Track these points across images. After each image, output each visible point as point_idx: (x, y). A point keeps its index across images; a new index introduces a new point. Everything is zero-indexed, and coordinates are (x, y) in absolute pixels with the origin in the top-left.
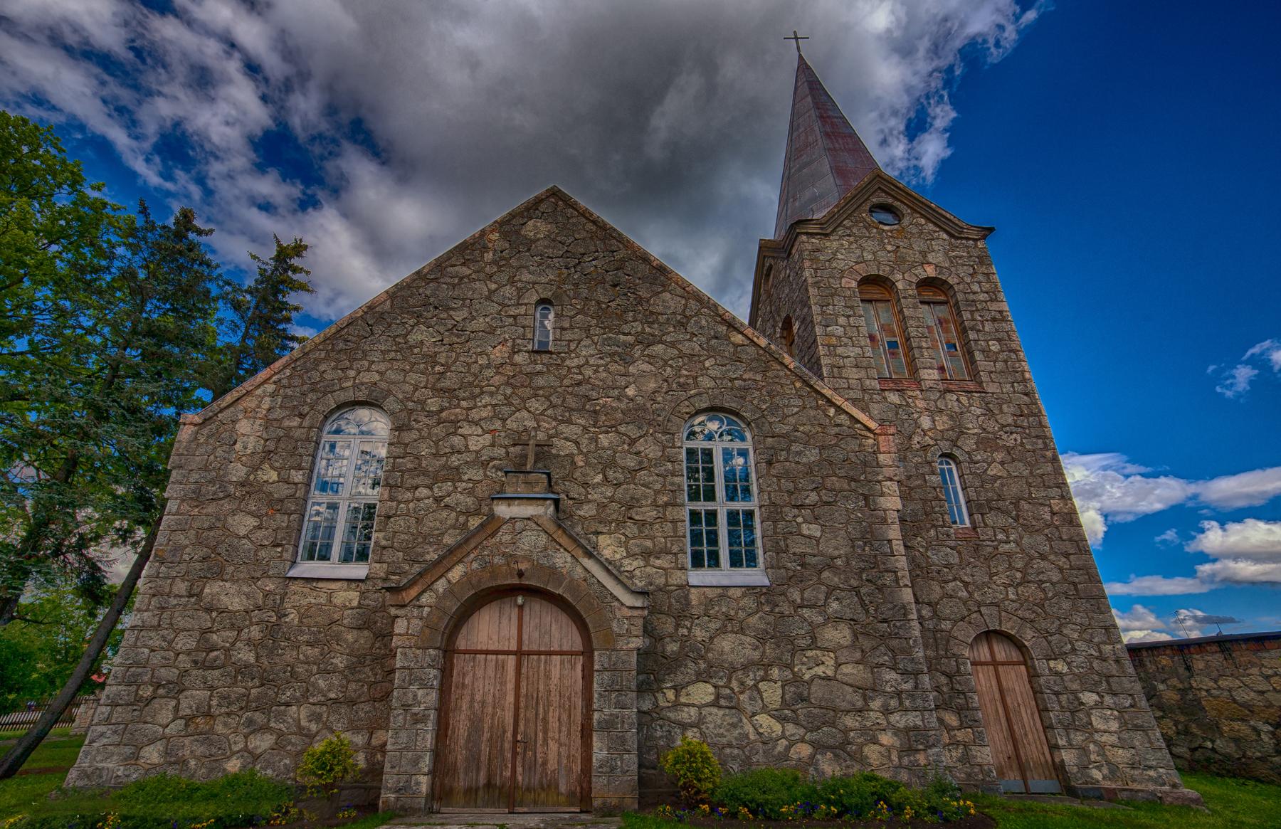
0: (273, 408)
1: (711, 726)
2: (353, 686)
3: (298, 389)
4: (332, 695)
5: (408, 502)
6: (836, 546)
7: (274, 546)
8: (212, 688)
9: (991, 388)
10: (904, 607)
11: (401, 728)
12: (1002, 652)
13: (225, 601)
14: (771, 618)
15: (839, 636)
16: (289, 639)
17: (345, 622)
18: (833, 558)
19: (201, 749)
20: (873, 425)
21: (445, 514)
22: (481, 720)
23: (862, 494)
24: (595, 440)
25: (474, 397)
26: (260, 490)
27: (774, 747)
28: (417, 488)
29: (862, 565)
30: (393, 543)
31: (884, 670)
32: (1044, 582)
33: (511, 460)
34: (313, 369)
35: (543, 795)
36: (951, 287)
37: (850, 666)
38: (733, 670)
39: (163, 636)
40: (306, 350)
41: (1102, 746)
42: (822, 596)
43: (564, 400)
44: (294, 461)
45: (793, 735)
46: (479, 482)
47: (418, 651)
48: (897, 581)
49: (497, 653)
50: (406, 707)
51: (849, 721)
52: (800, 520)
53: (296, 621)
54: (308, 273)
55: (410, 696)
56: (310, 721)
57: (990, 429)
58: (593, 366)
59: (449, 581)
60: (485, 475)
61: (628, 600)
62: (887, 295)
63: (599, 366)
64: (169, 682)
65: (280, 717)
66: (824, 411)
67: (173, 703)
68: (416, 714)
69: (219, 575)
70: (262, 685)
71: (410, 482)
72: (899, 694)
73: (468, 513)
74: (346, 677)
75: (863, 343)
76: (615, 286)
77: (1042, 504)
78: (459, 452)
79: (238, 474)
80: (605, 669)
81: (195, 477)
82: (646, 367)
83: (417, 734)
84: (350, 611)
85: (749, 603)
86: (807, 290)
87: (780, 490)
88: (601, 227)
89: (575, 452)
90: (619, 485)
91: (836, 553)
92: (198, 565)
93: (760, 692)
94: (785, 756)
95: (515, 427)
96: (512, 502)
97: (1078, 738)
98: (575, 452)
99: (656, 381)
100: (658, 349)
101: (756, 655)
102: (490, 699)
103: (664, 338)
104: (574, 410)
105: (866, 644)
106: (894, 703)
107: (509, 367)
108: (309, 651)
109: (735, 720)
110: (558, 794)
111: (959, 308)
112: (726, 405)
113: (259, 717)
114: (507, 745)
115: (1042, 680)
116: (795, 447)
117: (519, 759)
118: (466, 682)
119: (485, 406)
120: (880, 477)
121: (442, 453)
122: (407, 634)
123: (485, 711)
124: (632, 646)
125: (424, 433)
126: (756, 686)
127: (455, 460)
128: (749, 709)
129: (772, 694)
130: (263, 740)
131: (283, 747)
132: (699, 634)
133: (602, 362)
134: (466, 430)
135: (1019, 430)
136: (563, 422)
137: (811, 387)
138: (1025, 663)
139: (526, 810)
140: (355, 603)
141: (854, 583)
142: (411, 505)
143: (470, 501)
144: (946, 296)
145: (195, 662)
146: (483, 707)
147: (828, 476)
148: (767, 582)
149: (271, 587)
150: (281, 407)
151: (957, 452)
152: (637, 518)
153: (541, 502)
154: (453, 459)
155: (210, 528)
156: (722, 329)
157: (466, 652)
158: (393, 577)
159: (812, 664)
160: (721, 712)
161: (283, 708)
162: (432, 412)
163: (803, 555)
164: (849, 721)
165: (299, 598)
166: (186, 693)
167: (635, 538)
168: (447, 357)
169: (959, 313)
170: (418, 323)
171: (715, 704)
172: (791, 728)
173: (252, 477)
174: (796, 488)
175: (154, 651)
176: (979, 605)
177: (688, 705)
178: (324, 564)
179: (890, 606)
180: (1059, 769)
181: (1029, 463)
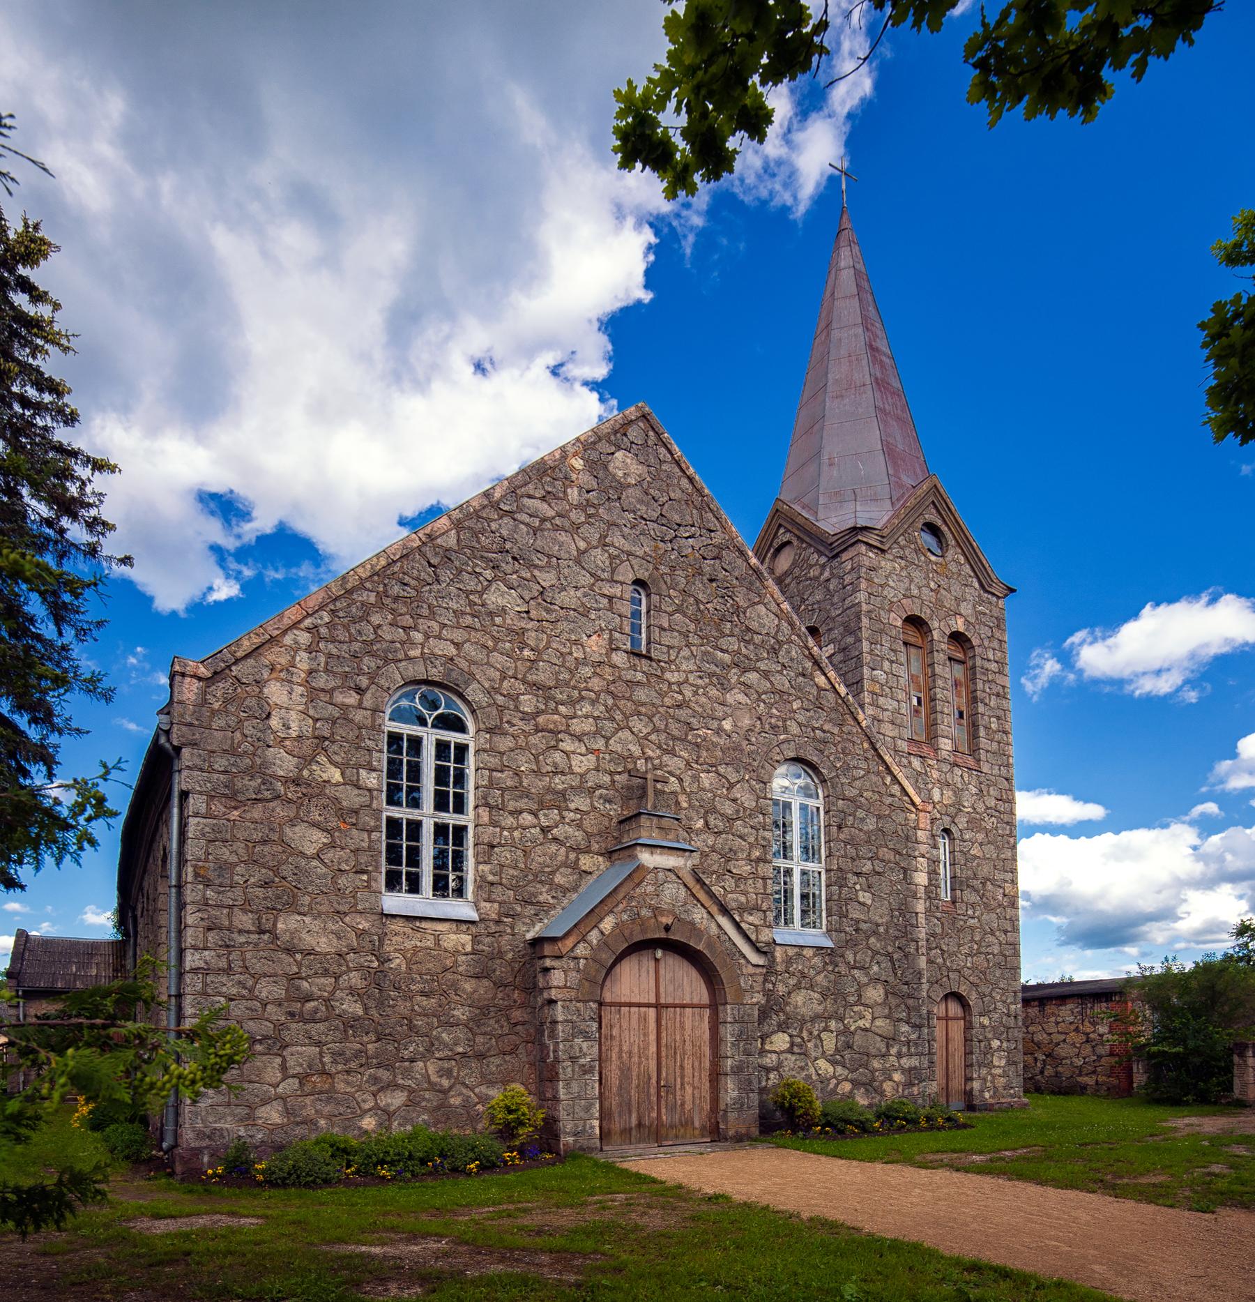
0: (316, 671)
1: (787, 1069)
2: (480, 1039)
3: (345, 647)
4: (460, 1050)
5: (511, 829)
6: (880, 915)
7: (356, 872)
8: (319, 1044)
9: (985, 768)
10: (920, 973)
11: (571, 1079)
12: (954, 1008)
13: (308, 940)
14: (832, 977)
15: (876, 995)
16: (400, 988)
17: (460, 969)
18: (878, 925)
19: (329, 1108)
20: (917, 800)
21: (553, 847)
22: (629, 1069)
23: (903, 868)
24: (696, 778)
25: (572, 703)
26: (321, 794)
27: (828, 1085)
28: (521, 812)
29: (897, 933)
30: (501, 878)
31: (902, 1024)
32: (989, 954)
33: (617, 790)
34: (361, 619)
35: (682, 1131)
36: (973, 647)
37: (880, 1020)
38: (803, 1022)
39: (240, 983)
40: (349, 586)
41: (993, 1076)
42: (868, 959)
43: (667, 725)
44: (362, 757)
45: (840, 1075)
46: (587, 813)
47: (578, 1004)
48: (917, 950)
49: (639, 1005)
50: (573, 1059)
51: (876, 1064)
52: (858, 887)
53: (404, 967)
54: (57, 307)
55: (577, 1048)
56: (441, 1076)
57: (978, 810)
58: (692, 685)
59: (602, 933)
60: (592, 805)
61: (755, 958)
62: (920, 641)
63: (698, 687)
64: (266, 1037)
65: (407, 1073)
66: (883, 779)
67: (278, 1060)
68: (583, 1066)
69: (292, 906)
70: (379, 1040)
71: (512, 805)
72: (908, 1042)
73: (578, 850)
74: (471, 1029)
75: (900, 697)
76: (711, 580)
77: (1000, 886)
78: (563, 773)
79: (285, 766)
80: (736, 1022)
81: (220, 763)
82: (741, 698)
83: (586, 1084)
84: (464, 957)
85: (817, 961)
86: (860, 619)
87: (845, 856)
88: (698, 490)
89: (679, 790)
90: (718, 833)
91: (880, 921)
92: (260, 892)
93: (822, 1041)
94: (834, 1091)
95: (619, 749)
96: (654, 850)
97: (984, 1071)
98: (679, 790)
99: (751, 718)
100: (752, 677)
101: (820, 1009)
102: (636, 1050)
103: (758, 664)
104: (678, 739)
105: (893, 1001)
106: (904, 1049)
107: (607, 669)
108: (424, 1001)
109: (803, 1064)
110: (694, 1129)
111: (975, 674)
112: (809, 758)
113: (384, 1075)
114: (653, 1091)
115: (974, 1032)
116: (860, 814)
117: (663, 1102)
118: (614, 1034)
119: (587, 717)
120: (917, 853)
121: (544, 771)
122: (565, 987)
123: (633, 1060)
124: (755, 1000)
125: (522, 741)
126: (819, 1035)
127: (559, 783)
128: (814, 1054)
129: (829, 1042)
130: (394, 1097)
131: (418, 1104)
132: (781, 989)
133: (700, 682)
134: (567, 745)
135: (997, 814)
136: (667, 752)
137: (876, 750)
138: (964, 1018)
139: (671, 1143)
140: (469, 948)
141: (890, 949)
142: (516, 834)
143: (579, 835)
144: (965, 654)
145: (292, 1014)
146: (630, 1057)
147: (881, 846)
148: (830, 944)
149: (363, 925)
150: (327, 671)
151: (954, 829)
152: (734, 871)
153: (680, 853)
154: (557, 781)
155: (264, 842)
156: (809, 664)
157: (612, 1004)
158: (505, 920)
159: (857, 1018)
160: (794, 1058)
161: (407, 1064)
162: (527, 714)
163: (858, 921)
164: (876, 1064)
165: (400, 941)
166: (290, 1049)
167: (732, 892)
168: (537, 639)
169: (974, 680)
170: (495, 578)
171: (790, 1051)
172: (839, 1069)
173: (305, 773)
174: (857, 856)
175: (232, 1000)
176: (949, 970)
177: (771, 1052)
178: (460, 901)
179: (911, 971)
180: (969, 1094)
181: (998, 846)
